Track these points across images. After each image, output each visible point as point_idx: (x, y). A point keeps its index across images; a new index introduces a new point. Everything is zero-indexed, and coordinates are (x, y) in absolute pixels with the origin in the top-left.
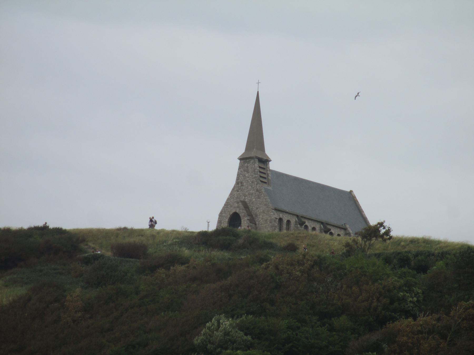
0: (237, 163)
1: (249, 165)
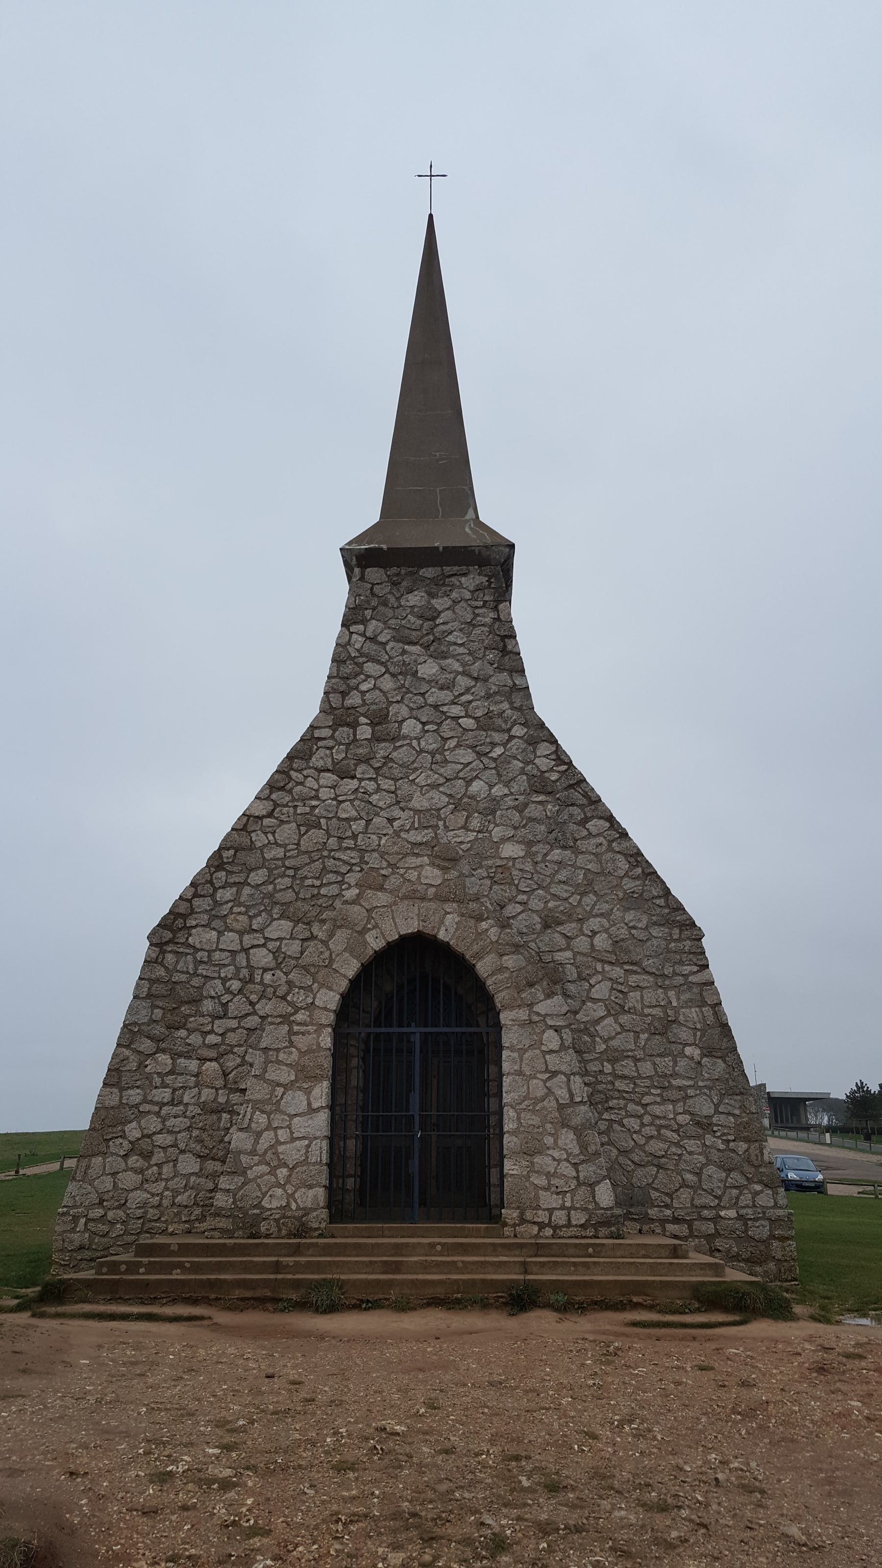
0: (331, 592)
1: (439, 603)
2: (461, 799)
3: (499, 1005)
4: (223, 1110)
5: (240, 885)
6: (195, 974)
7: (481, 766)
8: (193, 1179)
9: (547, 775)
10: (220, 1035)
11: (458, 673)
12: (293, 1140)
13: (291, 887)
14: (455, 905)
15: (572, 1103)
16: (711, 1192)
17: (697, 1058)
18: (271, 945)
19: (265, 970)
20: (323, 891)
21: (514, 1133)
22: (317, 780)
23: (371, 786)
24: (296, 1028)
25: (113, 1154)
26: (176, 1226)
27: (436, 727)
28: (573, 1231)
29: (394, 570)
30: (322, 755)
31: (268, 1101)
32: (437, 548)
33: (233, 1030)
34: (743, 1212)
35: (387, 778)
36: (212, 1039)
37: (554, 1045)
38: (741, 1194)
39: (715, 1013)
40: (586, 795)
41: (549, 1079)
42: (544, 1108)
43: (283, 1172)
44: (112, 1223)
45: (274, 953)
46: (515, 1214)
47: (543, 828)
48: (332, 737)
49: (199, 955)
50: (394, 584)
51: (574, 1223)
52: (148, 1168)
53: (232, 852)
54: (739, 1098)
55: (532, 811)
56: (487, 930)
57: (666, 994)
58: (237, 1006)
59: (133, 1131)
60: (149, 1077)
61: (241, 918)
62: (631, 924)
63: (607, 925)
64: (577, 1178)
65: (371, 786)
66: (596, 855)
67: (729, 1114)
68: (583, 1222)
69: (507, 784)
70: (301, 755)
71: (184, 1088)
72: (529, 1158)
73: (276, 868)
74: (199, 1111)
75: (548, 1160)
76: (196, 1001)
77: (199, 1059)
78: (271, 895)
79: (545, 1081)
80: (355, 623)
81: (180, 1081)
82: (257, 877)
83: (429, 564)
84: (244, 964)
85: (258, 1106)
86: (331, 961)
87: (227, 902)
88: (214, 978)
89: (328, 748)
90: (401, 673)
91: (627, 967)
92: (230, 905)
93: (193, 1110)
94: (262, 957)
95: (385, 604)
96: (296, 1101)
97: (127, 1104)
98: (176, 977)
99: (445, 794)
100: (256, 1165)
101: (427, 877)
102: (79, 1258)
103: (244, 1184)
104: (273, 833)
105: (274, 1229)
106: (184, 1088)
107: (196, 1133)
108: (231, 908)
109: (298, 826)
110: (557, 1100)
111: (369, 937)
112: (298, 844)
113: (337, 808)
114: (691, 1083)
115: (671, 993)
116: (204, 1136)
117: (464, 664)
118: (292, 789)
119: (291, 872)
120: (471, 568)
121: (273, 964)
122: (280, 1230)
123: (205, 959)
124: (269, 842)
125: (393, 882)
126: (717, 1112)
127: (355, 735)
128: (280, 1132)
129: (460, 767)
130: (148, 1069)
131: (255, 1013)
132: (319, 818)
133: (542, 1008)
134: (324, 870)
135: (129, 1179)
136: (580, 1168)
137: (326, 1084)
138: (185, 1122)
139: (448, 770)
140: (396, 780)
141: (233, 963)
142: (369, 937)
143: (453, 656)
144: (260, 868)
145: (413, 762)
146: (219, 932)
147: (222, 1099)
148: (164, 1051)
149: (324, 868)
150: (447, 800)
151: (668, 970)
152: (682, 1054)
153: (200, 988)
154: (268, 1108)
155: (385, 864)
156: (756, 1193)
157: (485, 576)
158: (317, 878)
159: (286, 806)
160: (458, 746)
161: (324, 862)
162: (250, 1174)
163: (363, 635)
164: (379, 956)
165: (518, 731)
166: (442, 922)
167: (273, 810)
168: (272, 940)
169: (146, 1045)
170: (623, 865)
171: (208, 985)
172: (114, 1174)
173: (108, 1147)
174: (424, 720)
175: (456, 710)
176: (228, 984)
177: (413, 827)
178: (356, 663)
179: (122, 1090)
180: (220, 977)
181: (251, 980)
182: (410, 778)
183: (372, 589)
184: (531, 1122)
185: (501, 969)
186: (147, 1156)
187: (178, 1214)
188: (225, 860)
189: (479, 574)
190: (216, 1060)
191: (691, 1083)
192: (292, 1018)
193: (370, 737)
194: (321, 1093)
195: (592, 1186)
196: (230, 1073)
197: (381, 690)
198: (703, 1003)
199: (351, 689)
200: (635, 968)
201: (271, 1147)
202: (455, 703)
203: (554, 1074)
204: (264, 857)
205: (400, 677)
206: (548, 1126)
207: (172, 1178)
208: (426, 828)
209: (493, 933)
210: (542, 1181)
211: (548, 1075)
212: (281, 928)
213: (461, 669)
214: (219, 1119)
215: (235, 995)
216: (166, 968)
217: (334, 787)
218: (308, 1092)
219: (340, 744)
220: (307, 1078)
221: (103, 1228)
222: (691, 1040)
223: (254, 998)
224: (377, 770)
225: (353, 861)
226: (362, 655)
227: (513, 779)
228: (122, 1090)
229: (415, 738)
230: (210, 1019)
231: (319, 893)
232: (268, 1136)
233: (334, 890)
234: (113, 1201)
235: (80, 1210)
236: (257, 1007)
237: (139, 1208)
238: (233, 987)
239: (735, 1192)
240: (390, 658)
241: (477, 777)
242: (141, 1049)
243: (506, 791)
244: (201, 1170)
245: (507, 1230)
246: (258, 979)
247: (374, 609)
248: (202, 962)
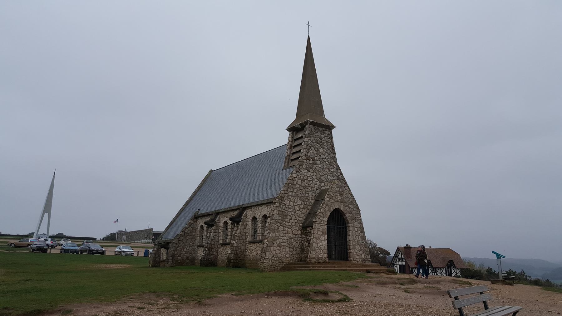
1: (323, 136)
23: (313, 174)
36: (290, 224)
58: (293, 218)
59: (278, 242)
65: (313, 174)
76: (286, 216)
81: (285, 232)
82: (295, 191)
83: (311, 124)
85: (317, 239)
94: (297, 208)
96: (322, 238)
125: (334, 198)
135: (278, 252)
165: (335, 166)
175: (326, 160)
186: (280, 247)
194: (326, 236)
212: (299, 202)
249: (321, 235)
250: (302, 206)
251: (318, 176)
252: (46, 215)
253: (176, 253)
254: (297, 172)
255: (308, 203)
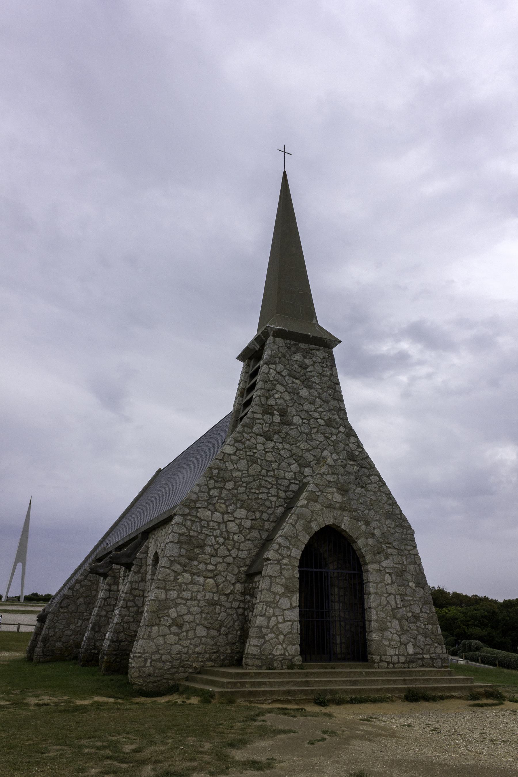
1: (308, 362)
2: (319, 458)
3: (367, 562)
4: (217, 604)
5: (221, 489)
6: (201, 533)
7: (327, 444)
8: (203, 639)
9: (354, 452)
10: (214, 565)
11: (317, 397)
12: (285, 621)
13: (245, 492)
14: (347, 513)
15: (397, 608)
16: (420, 647)
17: (414, 587)
18: (237, 521)
19: (235, 533)
20: (260, 496)
21: (376, 621)
22: (256, 439)
23: (280, 446)
24: (283, 567)
25: (163, 625)
26: (196, 663)
27: (307, 422)
28: (400, 665)
29: (288, 341)
30: (258, 427)
31: (272, 602)
32: (310, 336)
33: (221, 563)
34: (432, 655)
35: (287, 443)
36: (210, 567)
37: (389, 581)
38: (430, 647)
39: (419, 568)
40: (369, 464)
41: (388, 596)
42: (387, 610)
43: (281, 637)
44: (164, 662)
45: (238, 525)
46: (378, 658)
47: (353, 477)
48: (262, 419)
49: (203, 523)
50: (289, 348)
51: (401, 661)
52: (181, 633)
53: (217, 471)
54: (428, 605)
55: (349, 468)
56: (361, 526)
57: (402, 558)
58: (222, 551)
59: (173, 613)
60: (180, 585)
61: (222, 506)
62: (388, 526)
63: (379, 525)
64: (400, 641)
65: (280, 446)
66: (374, 492)
67: (426, 613)
68: (404, 661)
69: (338, 454)
70: (249, 426)
71: (197, 592)
72: (381, 632)
73: (238, 482)
74: (205, 604)
75: (389, 633)
76: (202, 547)
77: (204, 577)
78: (235, 496)
79: (386, 598)
80: (272, 364)
81: (195, 588)
82: (230, 485)
84: (224, 529)
85: (268, 604)
86: (297, 535)
87: (215, 497)
88: (210, 536)
89: (260, 424)
90: (292, 393)
91: (387, 545)
92: (217, 498)
93: (202, 603)
94: (233, 527)
95: (284, 357)
96: (285, 603)
97: (170, 599)
98: (192, 533)
99: (312, 455)
100: (269, 633)
101: (336, 498)
102: (148, 681)
103: (265, 643)
104: (236, 464)
105: (280, 666)
106: (198, 592)
107: (204, 615)
108: (218, 500)
109: (248, 461)
110: (391, 606)
111: (313, 524)
112: (247, 471)
113: (265, 455)
114: (411, 598)
115: (404, 558)
116: (208, 617)
117: (319, 393)
118: (244, 442)
119: (245, 485)
120: (321, 348)
121: (238, 531)
122: (282, 666)
123: (206, 525)
124: (234, 468)
125: (321, 499)
126: (421, 611)
127: (273, 419)
128: (279, 618)
129: (318, 443)
130: (179, 581)
131: (230, 555)
132: (257, 459)
133: (384, 564)
134: (260, 486)
136: (401, 637)
137: (298, 595)
138: (198, 610)
139: (314, 443)
140: (291, 445)
141: (219, 528)
142: (313, 524)
143: (315, 389)
144: (230, 481)
145: (299, 437)
146: (212, 512)
147: (216, 598)
148: (186, 571)
149: (260, 484)
150: (313, 458)
151: (402, 548)
152: (408, 585)
153: (204, 540)
154: (273, 605)
155: (318, 490)
156: (436, 647)
157: (327, 353)
158: (257, 489)
159: (242, 450)
160: (317, 432)
161: (260, 481)
162: (267, 638)
163: (275, 370)
164: (317, 533)
165: (342, 429)
166: (342, 520)
167: (236, 452)
168: (237, 518)
169: (178, 568)
170: (385, 498)
171: (207, 539)
172: (164, 636)
173: (160, 621)
174: (303, 417)
175: (316, 415)
176: (217, 539)
177: (328, 473)
178: (272, 384)
179: (166, 591)
180: (213, 535)
181: (228, 539)
182: (298, 445)
183: (278, 348)
184: (382, 616)
185: (367, 545)
186: (180, 626)
187: (198, 657)
188: (214, 475)
189: (324, 352)
190: (212, 578)
191: (411, 598)
192: (281, 562)
193: (279, 421)
194: (296, 598)
195: (406, 645)
196: (220, 585)
197: (284, 399)
198: (415, 563)
199: (271, 396)
200: (390, 546)
201: (276, 625)
202: (316, 411)
203: (390, 594)
204: (232, 475)
205: (292, 394)
206: (389, 618)
207: (194, 638)
208: (334, 474)
209: (363, 527)
210: (387, 643)
211: (387, 595)
212: (241, 513)
213: (317, 395)
214: (215, 608)
215: (221, 545)
216: (187, 528)
217: (264, 444)
218: (290, 599)
219: (266, 423)
220: (290, 592)
221: (160, 665)
222: (411, 579)
223: (230, 547)
224: (283, 438)
225: (273, 483)
226: (275, 380)
227: (340, 452)
228: (166, 591)
229: (299, 426)
230: (209, 557)
231: (258, 497)
232: (273, 619)
233: (264, 496)
234: (164, 650)
235: (148, 655)
236: (231, 552)
237: (177, 654)
238: (220, 541)
239: (428, 647)
240: (287, 384)
241: (325, 449)
242: (175, 570)
243: (338, 457)
244: (207, 634)
245: (376, 665)
246: (231, 538)
247: (280, 358)
248: (204, 527)
249: (282, 595)
250: (247, 524)
251: (295, 450)
252: (20, 565)
253: (52, 633)
254: (236, 441)
255: (265, 516)
